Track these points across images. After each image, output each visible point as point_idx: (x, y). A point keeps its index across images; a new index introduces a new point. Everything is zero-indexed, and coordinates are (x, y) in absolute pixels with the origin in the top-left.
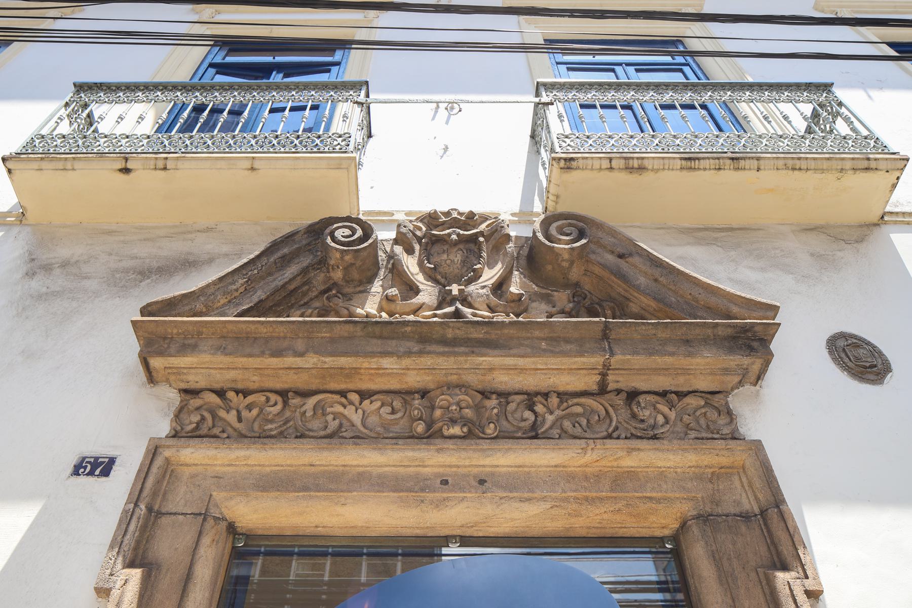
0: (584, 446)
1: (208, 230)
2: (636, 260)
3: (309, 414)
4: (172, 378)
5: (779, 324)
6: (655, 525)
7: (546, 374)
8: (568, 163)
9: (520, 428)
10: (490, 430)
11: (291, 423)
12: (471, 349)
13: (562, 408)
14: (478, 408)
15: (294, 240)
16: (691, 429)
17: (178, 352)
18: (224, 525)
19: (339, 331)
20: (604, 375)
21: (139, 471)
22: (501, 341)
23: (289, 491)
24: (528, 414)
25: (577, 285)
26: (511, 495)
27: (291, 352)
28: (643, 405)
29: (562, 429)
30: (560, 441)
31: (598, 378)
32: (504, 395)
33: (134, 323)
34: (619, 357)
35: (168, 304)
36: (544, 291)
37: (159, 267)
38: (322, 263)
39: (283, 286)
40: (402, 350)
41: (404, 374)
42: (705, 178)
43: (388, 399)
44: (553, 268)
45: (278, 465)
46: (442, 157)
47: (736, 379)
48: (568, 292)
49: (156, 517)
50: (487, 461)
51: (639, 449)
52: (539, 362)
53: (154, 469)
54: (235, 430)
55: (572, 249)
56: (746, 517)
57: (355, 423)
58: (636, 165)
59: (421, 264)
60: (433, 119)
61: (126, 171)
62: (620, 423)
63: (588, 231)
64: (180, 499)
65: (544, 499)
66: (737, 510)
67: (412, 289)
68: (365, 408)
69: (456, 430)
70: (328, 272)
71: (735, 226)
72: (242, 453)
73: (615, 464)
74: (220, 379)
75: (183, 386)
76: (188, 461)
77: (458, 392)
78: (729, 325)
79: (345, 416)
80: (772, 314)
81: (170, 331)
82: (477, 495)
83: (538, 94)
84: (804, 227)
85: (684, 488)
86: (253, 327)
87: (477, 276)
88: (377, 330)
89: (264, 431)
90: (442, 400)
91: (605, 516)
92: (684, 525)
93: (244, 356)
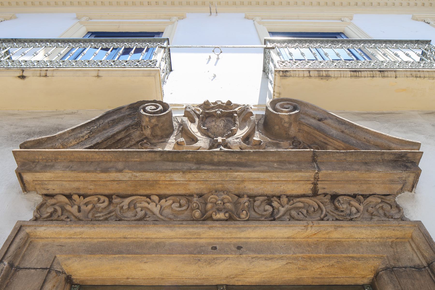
0: (306, 224)
1: (73, 113)
2: (329, 121)
3: (125, 207)
4: (38, 187)
5: (422, 153)
6: (358, 276)
7: (278, 184)
8: (285, 74)
9: (263, 216)
10: (243, 215)
11: (113, 213)
12: (230, 167)
13: (290, 204)
14: (236, 204)
15: (120, 112)
16: (375, 215)
17: (41, 169)
18: (63, 277)
19: (145, 157)
20: (315, 184)
21: (7, 240)
22: (248, 163)
23: (109, 254)
24: (268, 207)
25: (294, 137)
26: (259, 256)
27: (114, 169)
28: (342, 202)
29: (291, 216)
30: (290, 222)
31: (311, 186)
32: (252, 197)
33: (14, 152)
34: (323, 172)
35: (38, 143)
36: (275, 141)
37: (40, 131)
38: (138, 125)
39: (113, 136)
40: (185, 168)
41: (187, 184)
42: (365, 82)
43: (178, 199)
44: (279, 128)
45: (103, 238)
46: (212, 80)
47: (400, 187)
48: (289, 142)
49: (16, 270)
50: (242, 235)
51: (342, 227)
52: (274, 176)
53: (18, 240)
54: (76, 217)
55: (290, 115)
56: (418, 268)
57: (155, 213)
58: (324, 75)
59: (199, 128)
60: (208, 63)
61: (23, 77)
62: (328, 212)
63: (299, 107)
64: (34, 259)
65: (281, 258)
66: (412, 264)
67: (195, 140)
68: (162, 205)
69: (221, 215)
70: (142, 131)
71: (385, 112)
72: (78, 230)
73: (327, 236)
74: (69, 187)
75: (45, 192)
76: (42, 235)
77: (222, 194)
78: (391, 153)
79: (148, 209)
80: (417, 147)
81: (37, 157)
82: (236, 256)
83: (265, 44)
84: (426, 112)
85: (374, 251)
86: (90, 155)
87: (233, 133)
88: (170, 156)
89: (95, 217)
90: (212, 198)
91: (323, 270)
92: (377, 275)
93: (84, 172)
